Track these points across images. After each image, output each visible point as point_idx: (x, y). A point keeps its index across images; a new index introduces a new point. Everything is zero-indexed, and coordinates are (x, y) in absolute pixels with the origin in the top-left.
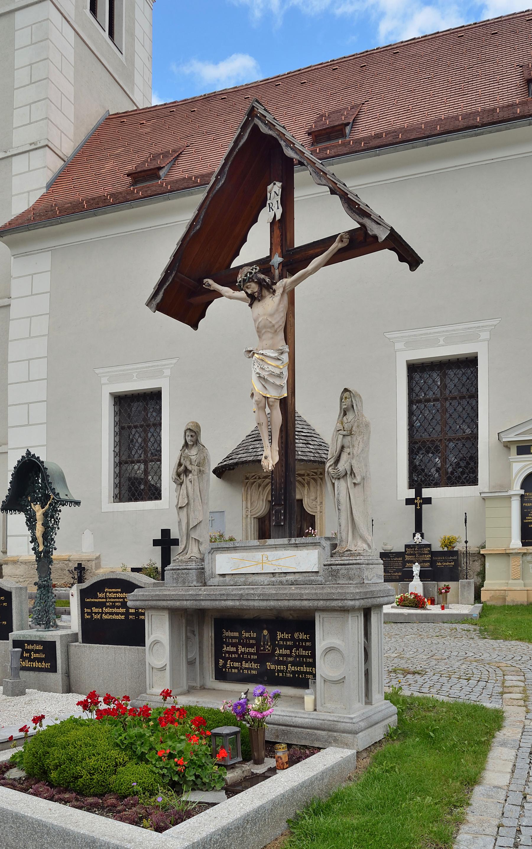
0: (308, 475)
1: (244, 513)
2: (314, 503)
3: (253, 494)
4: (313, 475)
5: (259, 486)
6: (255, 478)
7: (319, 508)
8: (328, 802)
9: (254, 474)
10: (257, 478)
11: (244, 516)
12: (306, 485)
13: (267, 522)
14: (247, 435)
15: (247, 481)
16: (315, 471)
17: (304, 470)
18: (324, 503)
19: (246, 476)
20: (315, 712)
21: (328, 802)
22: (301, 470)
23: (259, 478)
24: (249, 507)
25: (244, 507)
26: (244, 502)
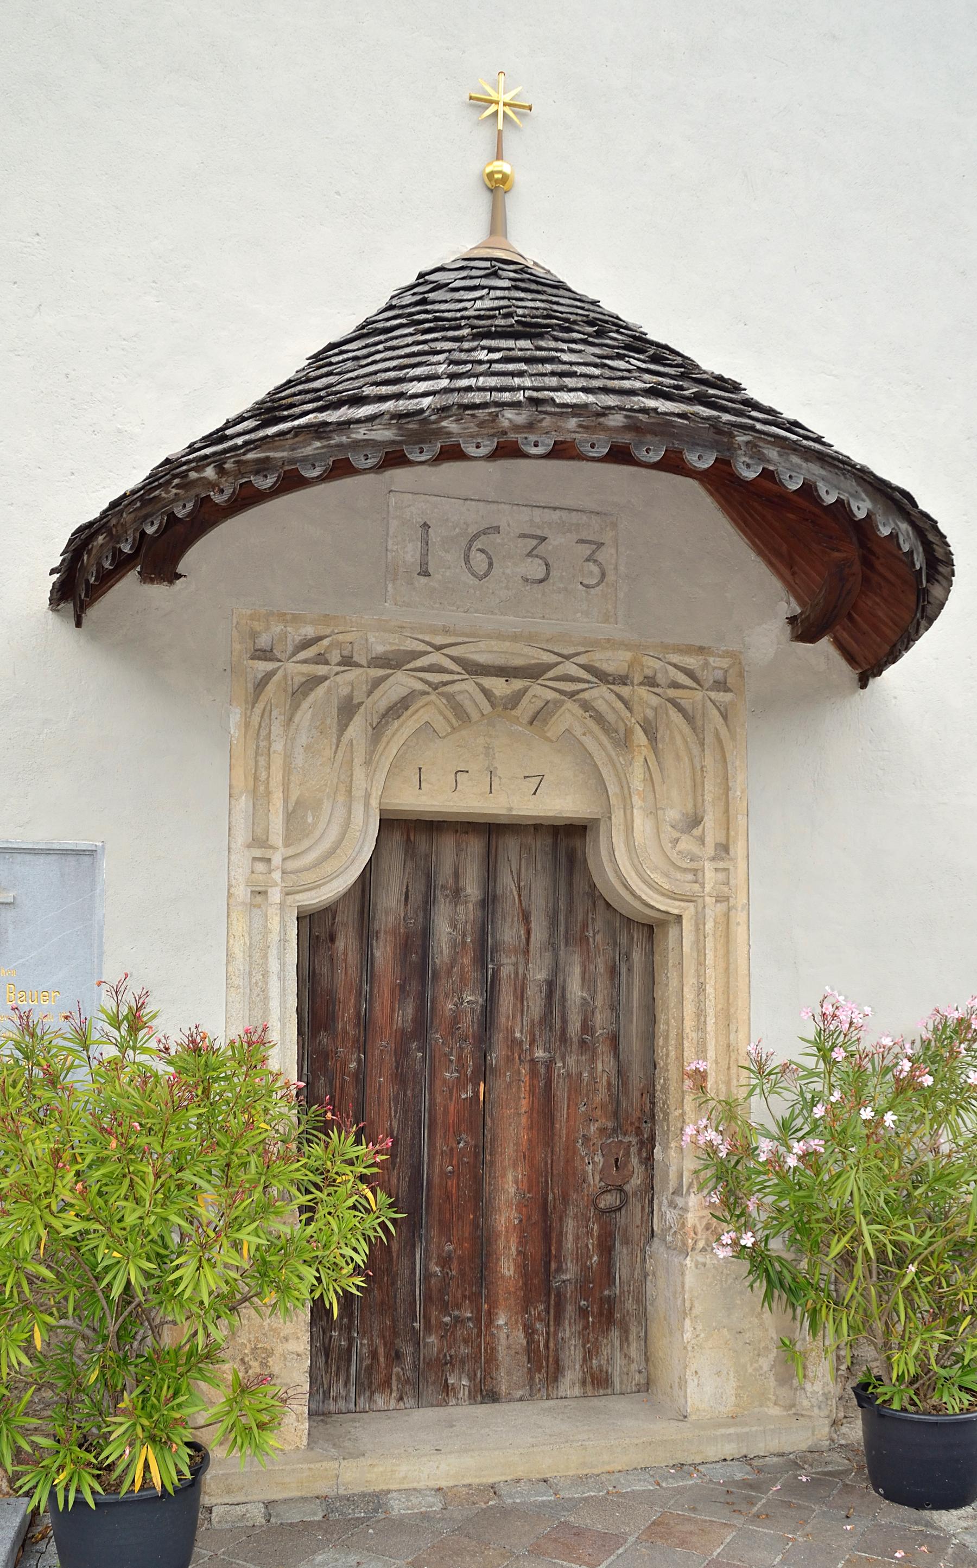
0: (650, 682)
1: (241, 873)
2: (687, 844)
3: (299, 759)
4: (675, 685)
5: (348, 710)
6: (320, 659)
7: (710, 876)
8: (447, 896)
9: (310, 631)
10: (335, 657)
11: (242, 892)
12: (640, 737)
13: (346, 943)
14: (298, 369)
15: (263, 667)
16: (691, 662)
17: (627, 646)
18: (738, 849)
19: (254, 635)
20: (423, 580)
21: (447, 896)
22: (611, 644)
23: (348, 662)
24: (277, 837)
25: (241, 837)
26: (243, 803)
